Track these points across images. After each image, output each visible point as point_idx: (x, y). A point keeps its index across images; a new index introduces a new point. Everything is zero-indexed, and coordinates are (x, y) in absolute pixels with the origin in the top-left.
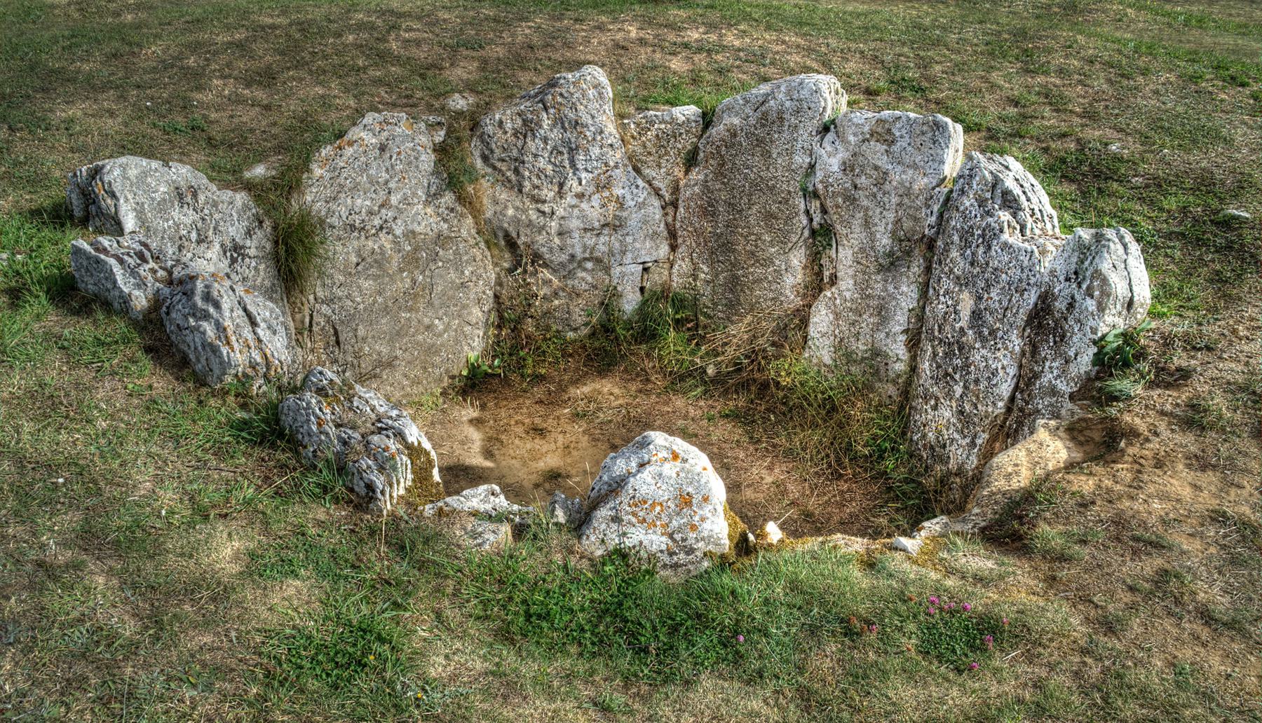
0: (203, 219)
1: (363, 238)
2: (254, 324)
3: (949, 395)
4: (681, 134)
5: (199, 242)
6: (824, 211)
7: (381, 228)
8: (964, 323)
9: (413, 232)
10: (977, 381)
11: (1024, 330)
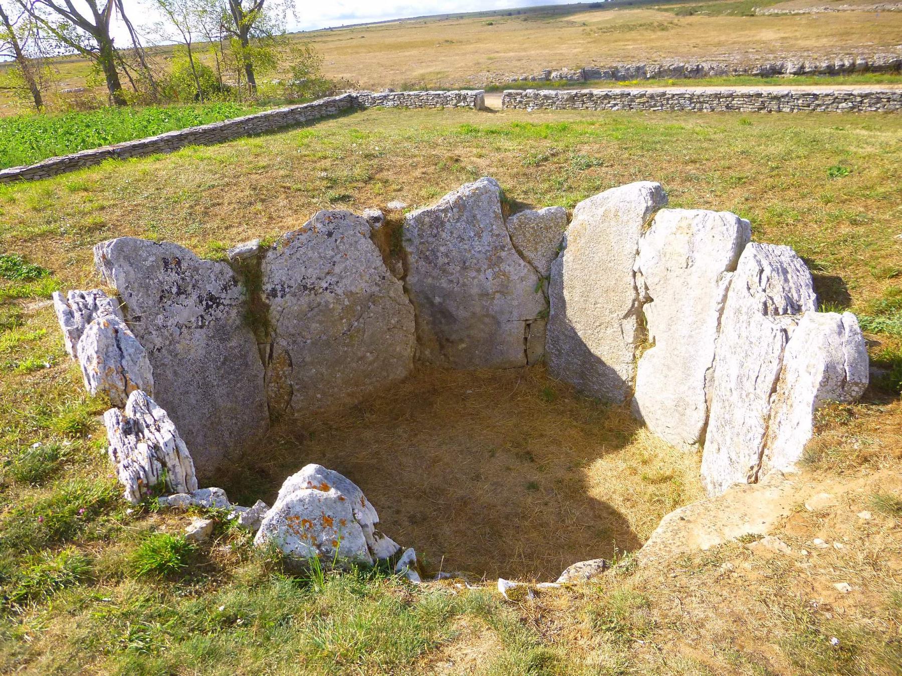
1: (313, 295)
4: (551, 227)
5: (179, 293)
6: (647, 288)
7: (327, 289)
8: (733, 385)
9: (351, 292)
10: (738, 434)
11: (770, 396)
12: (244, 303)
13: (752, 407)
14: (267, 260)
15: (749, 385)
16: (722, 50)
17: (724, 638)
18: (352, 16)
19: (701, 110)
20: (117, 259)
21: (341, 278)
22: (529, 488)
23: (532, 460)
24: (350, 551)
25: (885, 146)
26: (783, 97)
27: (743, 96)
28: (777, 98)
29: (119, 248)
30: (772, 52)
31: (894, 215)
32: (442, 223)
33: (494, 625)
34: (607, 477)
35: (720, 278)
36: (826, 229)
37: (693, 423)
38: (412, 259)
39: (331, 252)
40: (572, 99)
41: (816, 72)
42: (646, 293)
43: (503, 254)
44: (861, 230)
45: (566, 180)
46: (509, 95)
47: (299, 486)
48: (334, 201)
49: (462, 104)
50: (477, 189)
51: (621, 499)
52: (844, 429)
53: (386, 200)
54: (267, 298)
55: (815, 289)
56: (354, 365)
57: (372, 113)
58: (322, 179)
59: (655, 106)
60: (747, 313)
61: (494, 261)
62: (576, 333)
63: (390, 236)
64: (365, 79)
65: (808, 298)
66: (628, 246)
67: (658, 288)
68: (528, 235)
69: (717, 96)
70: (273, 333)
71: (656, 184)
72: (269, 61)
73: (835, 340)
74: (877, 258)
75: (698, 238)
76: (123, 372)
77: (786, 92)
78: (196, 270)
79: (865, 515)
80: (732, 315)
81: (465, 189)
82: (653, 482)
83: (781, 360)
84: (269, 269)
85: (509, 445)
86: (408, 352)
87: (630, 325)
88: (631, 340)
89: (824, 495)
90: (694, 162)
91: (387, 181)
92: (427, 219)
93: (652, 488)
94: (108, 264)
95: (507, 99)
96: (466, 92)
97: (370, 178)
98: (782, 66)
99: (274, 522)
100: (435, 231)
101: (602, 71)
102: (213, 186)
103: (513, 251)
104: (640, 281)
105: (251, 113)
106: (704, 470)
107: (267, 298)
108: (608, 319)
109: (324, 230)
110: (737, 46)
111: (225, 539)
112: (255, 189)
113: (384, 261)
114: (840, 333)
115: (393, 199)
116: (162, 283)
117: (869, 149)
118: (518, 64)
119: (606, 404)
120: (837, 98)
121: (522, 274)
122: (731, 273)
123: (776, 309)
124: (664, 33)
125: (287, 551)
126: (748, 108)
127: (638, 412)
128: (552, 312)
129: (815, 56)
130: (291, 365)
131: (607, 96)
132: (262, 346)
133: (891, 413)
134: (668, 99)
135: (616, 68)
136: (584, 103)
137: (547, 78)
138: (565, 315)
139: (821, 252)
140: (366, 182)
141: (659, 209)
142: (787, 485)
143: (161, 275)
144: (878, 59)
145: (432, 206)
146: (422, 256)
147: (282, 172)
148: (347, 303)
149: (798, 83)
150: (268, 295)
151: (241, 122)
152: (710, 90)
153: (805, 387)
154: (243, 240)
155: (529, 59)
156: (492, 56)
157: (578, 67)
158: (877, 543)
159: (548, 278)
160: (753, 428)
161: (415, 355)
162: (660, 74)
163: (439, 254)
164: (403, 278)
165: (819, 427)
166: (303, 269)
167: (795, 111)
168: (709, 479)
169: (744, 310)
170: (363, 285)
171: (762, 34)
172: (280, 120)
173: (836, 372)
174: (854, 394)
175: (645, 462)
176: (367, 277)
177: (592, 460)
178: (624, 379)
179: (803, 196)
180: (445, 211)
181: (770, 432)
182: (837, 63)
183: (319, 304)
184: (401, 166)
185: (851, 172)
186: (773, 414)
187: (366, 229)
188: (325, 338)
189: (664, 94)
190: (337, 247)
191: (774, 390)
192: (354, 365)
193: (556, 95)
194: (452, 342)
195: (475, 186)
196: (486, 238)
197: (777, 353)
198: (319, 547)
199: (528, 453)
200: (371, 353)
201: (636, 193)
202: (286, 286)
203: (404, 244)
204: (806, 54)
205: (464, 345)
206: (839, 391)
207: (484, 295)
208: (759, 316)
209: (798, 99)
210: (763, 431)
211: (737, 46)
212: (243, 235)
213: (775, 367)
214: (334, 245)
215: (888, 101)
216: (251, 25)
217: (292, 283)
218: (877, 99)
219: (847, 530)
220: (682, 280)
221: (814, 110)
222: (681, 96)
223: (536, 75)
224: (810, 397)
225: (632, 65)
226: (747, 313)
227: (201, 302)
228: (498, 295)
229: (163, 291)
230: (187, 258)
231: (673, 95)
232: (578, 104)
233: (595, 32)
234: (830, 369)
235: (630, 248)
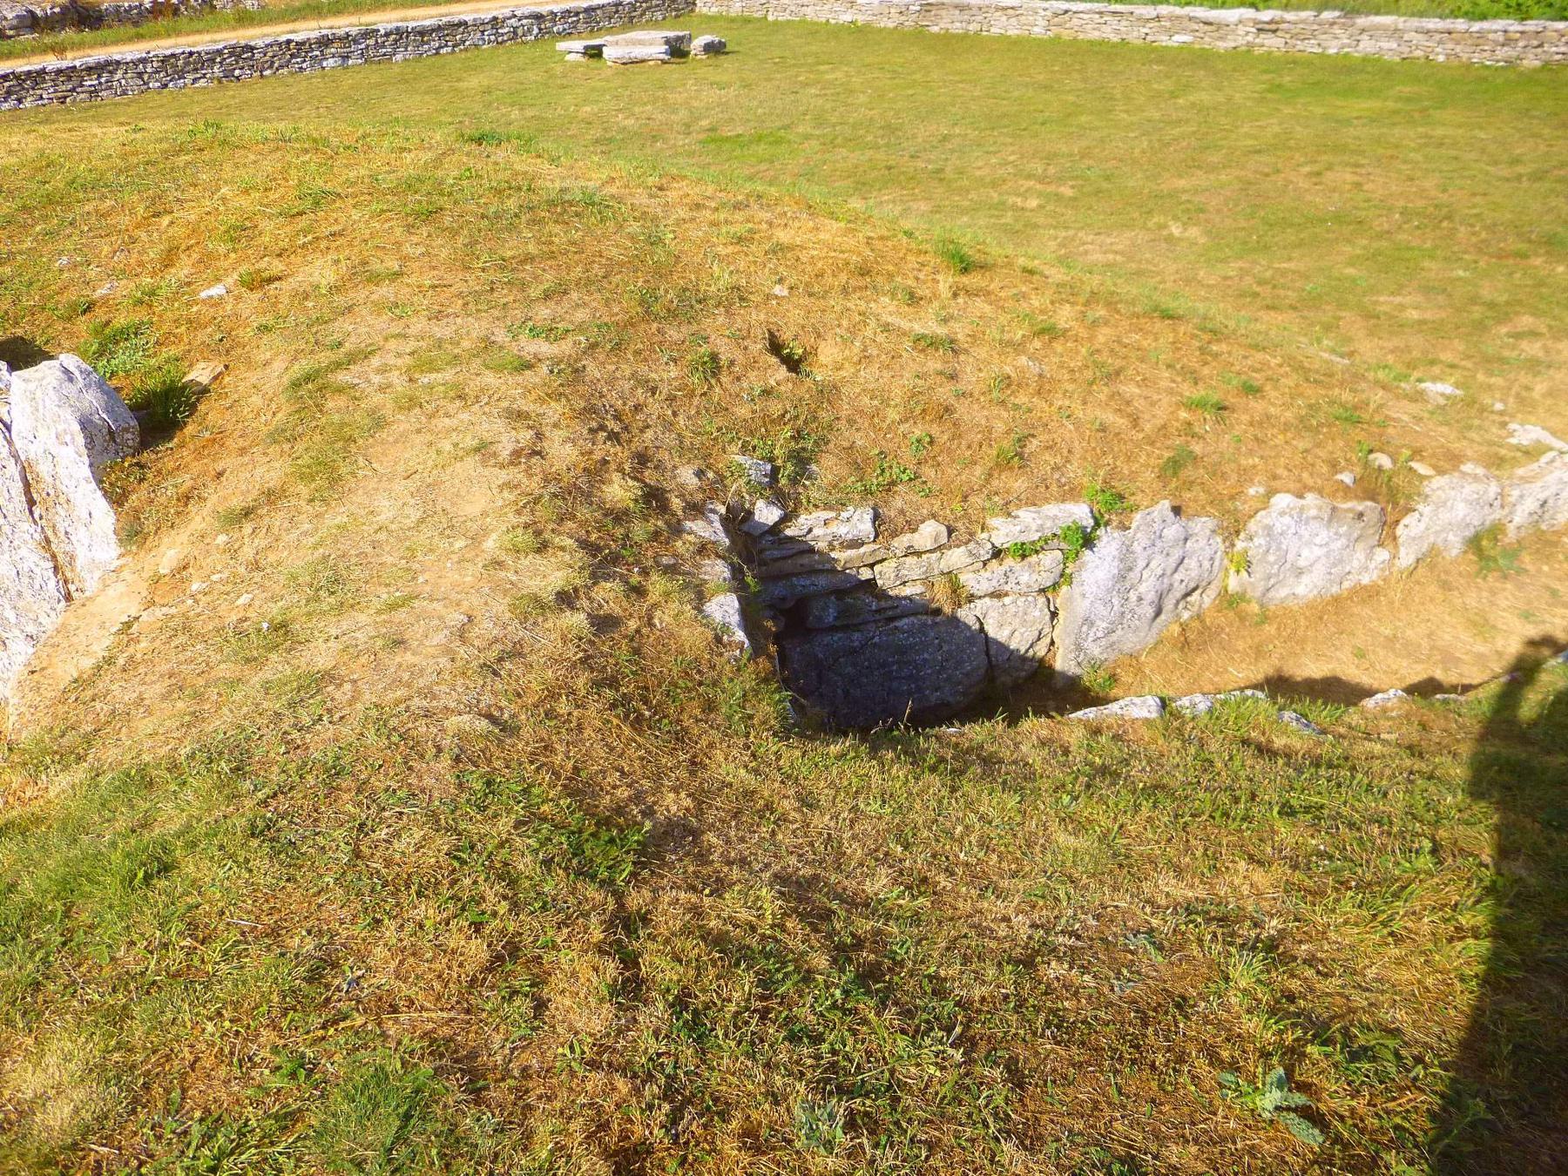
10: (20, 594)
13: (16, 543)
17: (170, 693)
31: (35, 240)
52: (145, 485)
73: (71, 389)
79: (222, 539)
83: (16, 457)
89: (172, 552)
114: (71, 380)
133: (182, 445)
142: (126, 574)
153: (69, 467)
158: (248, 552)
160: (37, 570)
165: (117, 499)
174: (130, 443)
181: (60, 557)
186: (50, 533)
191: (31, 503)
206: (112, 447)
210: (51, 564)
213: (13, 470)
219: (217, 560)
234: (85, 424)
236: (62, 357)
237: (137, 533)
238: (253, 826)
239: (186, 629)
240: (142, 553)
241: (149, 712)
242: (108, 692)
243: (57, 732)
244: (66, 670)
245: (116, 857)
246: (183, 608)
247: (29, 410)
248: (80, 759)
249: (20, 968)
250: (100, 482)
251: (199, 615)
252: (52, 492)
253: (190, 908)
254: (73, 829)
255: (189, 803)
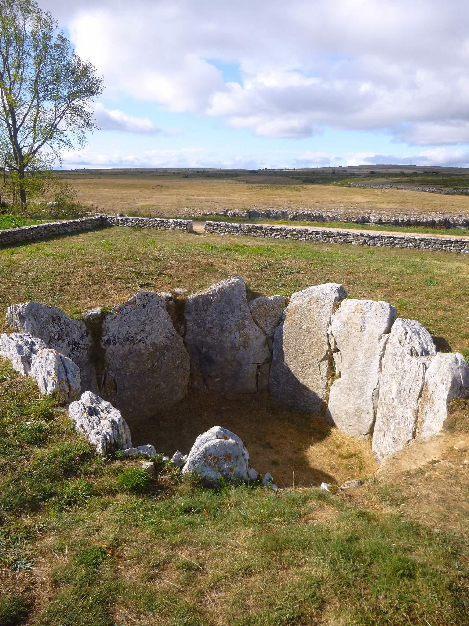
0: (61, 330)
1: (132, 344)
2: (67, 372)
3: (389, 430)
4: (275, 308)
6: (336, 343)
7: (140, 340)
8: (394, 396)
9: (154, 343)
10: (399, 423)
11: (418, 399)
12: (91, 347)
14: (107, 320)
15: (404, 394)
16: (334, 205)
17: (440, 501)
18: (83, 163)
19: (329, 241)
20: (28, 315)
21: (149, 334)
22: (272, 464)
23: (271, 448)
24: (239, 473)
25: (450, 270)
26: (376, 237)
27: (353, 235)
28: (372, 238)
29: (30, 308)
30: (363, 209)
31: (464, 306)
32: (211, 303)
33: (329, 503)
34: (317, 455)
35: (381, 337)
36: (431, 313)
37: (366, 421)
38: (189, 324)
39: (144, 318)
40: (250, 229)
41: (388, 223)
42: (335, 346)
43: (246, 323)
44: (450, 314)
45: (280, 281)
46: (209, 224)
47: (209, 438)
48: (142, 286)
49: (178, 228)
50: (233, 283)
51: (329, 468)
53: (174, 287)
54: (104, 345)
55: (435, 343)
56: (154, 390)
57: (116, 230)
58: (132, 272)
59: (301, 237)
60: (401, 356)
61: (241, 327)
62: (290, 371)
63: (178, 308)
64: (103, 206)
65: (432, 348)
66: (324, 319)
67: (343, 343)
68: (261, 311)
69: (339, 234)
70: (106, 368)
71: (341, 285)
72: (38, 189)
73: (454, 366)
74: (461, 328)
75: (367, 315)
76: (68, 381)
77: (378, 235)
78: (68, 325)
80: (390, 357)
81: (225, 283)
82: (346, 458)
83: (423, 379)
84: (107, 326)
85: (255, 439)
86: (185, 383)
87: (325, 366)
88: (325, 374)
89: (462, 442)
90: (352, 273)
91: (171, 276)
92: (201, 300)
93: (345, 461)
94: (22, 318)
95: (208, 227)
96: (181, 220)
97: (161, 273)
98: (369, 218)
99: (196, 459)
100: (205, 307)
101: (261, 212)
102: (62, 273)
103: (252, 321)
104: (332, 340)
105: (35, 224)
106: (374, 447)
107: (104, 345)
108: (310, 362)
109: (141, 303)
110: (342, 204)
111: (165, 473)
112: (90, 276)
113: (174, 325)
115: (177, 287)
116: (50, 332)
117: (443, 272)
118: (207, 204)
119: (309, 414)
120: (406, 240)
121: (257, 335)
122: (387, 335)
123: (417, 354)
124: (298, 193)
125: (203, 475)
126: (356, 243)
127: (330, 417)
128: (274, 359)
129: (388, 214)
130: (116, 389)
131: (271, 230)
132: (99, 376)
134: (309, 234)
135: (269, 211)
136: (257, 232)
137: (225, 215)
138: (283, 361)
139: (431, 325)
140: (158, 275)
141: (343, 299)
142: (441, 440)
143: (50, 327)
144: (423, 218)
145: (204, 292)
146: (196, 322)
147: (104, 267)
148: (151, 350)
149: (377, 229)
150: (105, 343)
151: (28, 230)
152: (334, 230)
153: (441, 392)
154: (90, 308)
155: (213, 201)
156: (189, 197)
157: (245, 209)
159: (272, 338)
160: (409, 419)
161: (188, 386)
162: (296, 218)
163: (207, 322)
164: (183, 336)
165: (451, 410)
166: (127, 328)
167: (383, 246)
168: (379, 453)
169: (399, 354)
170: (162, 339)
171: (356, 199)
172: (54, 230)
173: (457, 382)
174: (466, 393)
175: (338, 447)
176: (164, 335)
177: (307, 447)
178: (321, 397)
179: (415, 295)
180: (213, 295)
181: (419, 419)
182: (400, 219)
183: (136, 350)
184: (178, 267)
185: (437, 283)
186: (420, 409)
187: (164, 304)
188: (137, 372)
189: (307, 231)
190: (148, 314)
191: (420, 396)
192: (154, 390)
193: (240, 226)
194: (211, 377)
195: (231, 282)
196: (237, 313)
197: (421, 376)
198: (221, 472)
199: (268, 444)
200: (164, 383)
201: (329, 289)
202: (116, 338)
203: (185, 314)
204: (382, 212)
205: (218, 379)
206: (459, 392)
207: (233, 347)
208: (409, 357)
209: (385, 239)
211: (342, 204)
212: (89, 305)
213: (420, 383)
214: (146, 313)
215: (435, 244)
216: (27, 164)
217: (120, 336)
218: (429, 242)
220: (358, 339)
221: (394, 246)
222: (317, 232)
223: (218, 211)
224: (445, 395)
225: (279, 210)
226: (401, 356)
227: (69, 345)
228: (241, 348)
229: (50, 337)
230: (64, 317)
231: (312, 232)
232: (253, 233)
233: (255, 188)
234: (455, 381)
235: (325, 320)
236: (457, 353)
237: (452, 428)
238: (451, 586)
239: (456, 477)
240: (450, 436)
241: (429, 503)
242: (417, 485)
243: (394, 489)
244: (407, 465)
245: (395, 558)
246: (458, 467)
247: (437, 367)
248: (398, 505)
249: (347, 573)
250: (448, 402)
251: (462, 474)
252: (429, 397)
253: (412, 601)
254: (385, 532)
255: (430, 554)
